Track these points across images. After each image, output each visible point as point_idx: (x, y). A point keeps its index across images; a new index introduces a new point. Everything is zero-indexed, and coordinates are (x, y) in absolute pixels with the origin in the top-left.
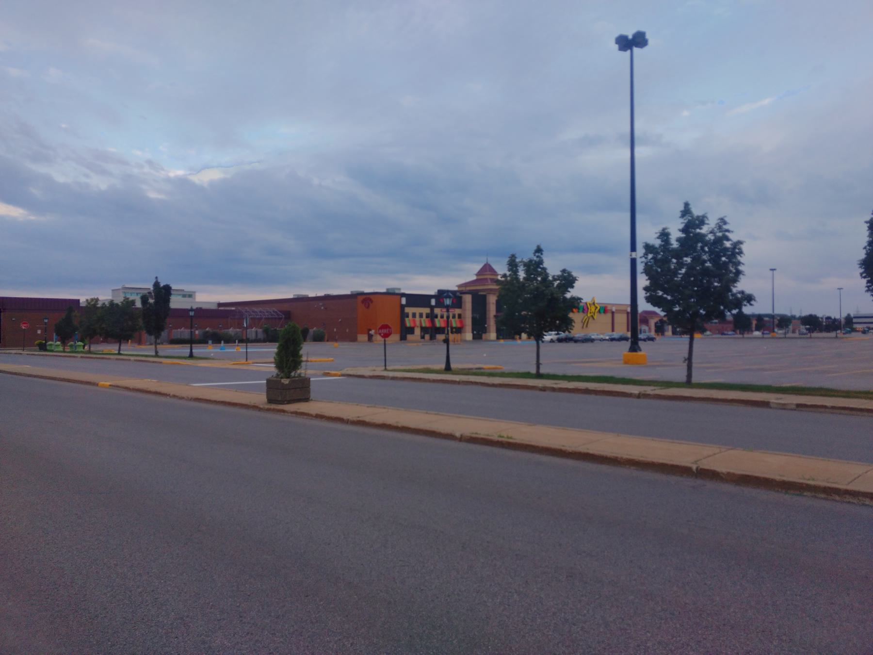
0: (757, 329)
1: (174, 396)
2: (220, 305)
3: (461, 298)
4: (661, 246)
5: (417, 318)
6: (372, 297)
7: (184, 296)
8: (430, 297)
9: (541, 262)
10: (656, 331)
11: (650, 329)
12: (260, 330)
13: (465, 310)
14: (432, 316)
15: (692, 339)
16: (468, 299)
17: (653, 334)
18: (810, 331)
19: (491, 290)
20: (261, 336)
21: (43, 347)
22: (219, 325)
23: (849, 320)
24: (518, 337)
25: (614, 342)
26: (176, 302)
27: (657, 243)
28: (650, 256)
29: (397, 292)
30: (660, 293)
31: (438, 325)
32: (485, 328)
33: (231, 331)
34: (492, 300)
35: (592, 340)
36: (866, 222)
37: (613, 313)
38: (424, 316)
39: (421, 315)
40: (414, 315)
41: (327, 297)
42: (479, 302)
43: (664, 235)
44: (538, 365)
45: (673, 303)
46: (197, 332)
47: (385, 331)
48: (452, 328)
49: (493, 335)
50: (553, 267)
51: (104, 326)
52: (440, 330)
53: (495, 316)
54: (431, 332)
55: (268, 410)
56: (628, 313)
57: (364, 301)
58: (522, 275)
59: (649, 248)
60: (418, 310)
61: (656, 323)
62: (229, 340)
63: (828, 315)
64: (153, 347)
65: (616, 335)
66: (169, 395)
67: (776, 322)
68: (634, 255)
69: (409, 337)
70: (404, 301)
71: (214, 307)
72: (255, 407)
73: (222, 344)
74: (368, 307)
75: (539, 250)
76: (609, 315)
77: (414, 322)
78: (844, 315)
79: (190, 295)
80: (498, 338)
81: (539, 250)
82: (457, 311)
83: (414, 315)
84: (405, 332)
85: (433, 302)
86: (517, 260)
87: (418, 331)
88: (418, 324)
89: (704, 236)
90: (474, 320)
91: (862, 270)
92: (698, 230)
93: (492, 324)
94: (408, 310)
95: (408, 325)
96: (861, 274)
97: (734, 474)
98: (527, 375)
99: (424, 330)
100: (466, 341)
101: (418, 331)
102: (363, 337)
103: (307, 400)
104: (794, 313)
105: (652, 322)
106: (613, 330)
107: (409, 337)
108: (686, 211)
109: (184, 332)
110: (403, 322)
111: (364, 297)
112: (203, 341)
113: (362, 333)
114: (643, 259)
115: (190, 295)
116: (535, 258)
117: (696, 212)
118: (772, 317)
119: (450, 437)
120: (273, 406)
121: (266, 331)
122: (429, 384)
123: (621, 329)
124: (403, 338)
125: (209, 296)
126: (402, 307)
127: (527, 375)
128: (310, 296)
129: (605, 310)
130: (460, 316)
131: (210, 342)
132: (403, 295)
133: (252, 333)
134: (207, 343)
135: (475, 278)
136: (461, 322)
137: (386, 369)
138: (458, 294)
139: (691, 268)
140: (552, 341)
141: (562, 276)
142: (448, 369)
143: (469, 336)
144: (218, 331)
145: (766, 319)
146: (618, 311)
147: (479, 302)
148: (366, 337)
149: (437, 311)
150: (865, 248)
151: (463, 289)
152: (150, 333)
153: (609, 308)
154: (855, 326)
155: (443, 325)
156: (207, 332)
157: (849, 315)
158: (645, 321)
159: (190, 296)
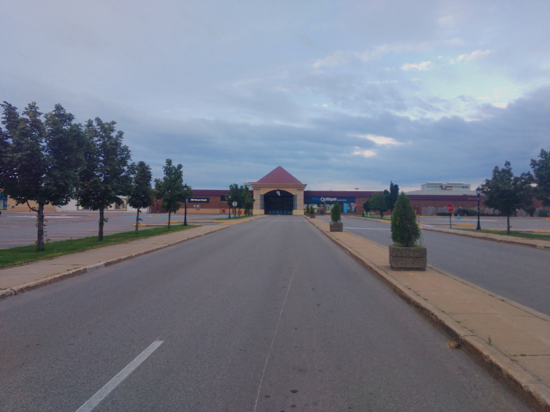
7: (463, 187)
15: (169, 223)
21: (363, 215)
22: (339, 205)
44: (509, 227)
47: (450, 208)
64: (171, 224)
73: (459, 216)
79: (467, 187)
98: (501, 233)
115: (467, 187)
116: (505, 168)
127: (501, 233)
137: (451, 228)
142: (479, 228)
144: (465, 208)
159: (467, 187)
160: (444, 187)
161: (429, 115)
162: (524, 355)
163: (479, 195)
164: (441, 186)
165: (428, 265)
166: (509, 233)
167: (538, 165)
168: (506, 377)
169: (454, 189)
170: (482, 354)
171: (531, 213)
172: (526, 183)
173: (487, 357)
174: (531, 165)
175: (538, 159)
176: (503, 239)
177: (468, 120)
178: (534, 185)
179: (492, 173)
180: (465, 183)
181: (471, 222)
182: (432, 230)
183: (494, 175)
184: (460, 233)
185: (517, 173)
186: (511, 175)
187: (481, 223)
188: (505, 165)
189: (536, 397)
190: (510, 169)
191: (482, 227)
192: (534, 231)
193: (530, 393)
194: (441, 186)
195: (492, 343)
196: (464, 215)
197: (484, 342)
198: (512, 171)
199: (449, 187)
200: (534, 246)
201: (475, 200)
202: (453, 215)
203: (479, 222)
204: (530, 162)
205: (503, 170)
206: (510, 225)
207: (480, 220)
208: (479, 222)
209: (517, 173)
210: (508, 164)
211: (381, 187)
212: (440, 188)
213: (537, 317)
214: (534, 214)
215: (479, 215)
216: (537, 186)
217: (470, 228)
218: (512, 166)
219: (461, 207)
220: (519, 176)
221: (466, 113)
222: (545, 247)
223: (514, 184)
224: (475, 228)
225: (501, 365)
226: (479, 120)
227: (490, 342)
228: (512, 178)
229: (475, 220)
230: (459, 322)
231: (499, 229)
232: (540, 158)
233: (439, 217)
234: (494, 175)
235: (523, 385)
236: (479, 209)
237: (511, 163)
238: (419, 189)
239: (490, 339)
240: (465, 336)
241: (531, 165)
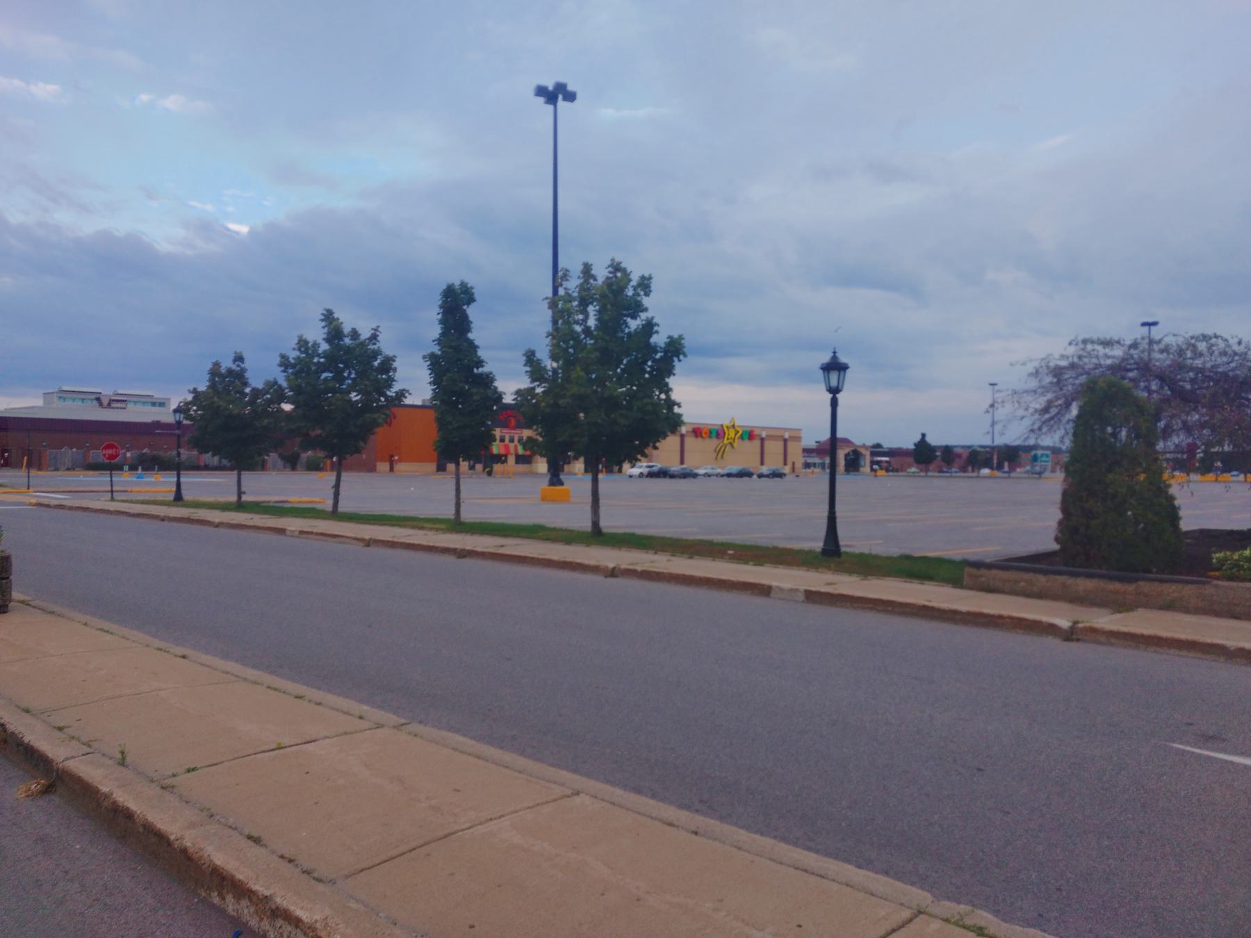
7: (154, 404)
24: (616, 468)
25: (731, 479)
35: (695, 476)
37: (762, 440)
46: (128, 455)
47: (110, 452)
61: (846, 456)
65: (765, 470)
76: (757, 443)
77: (507, 447)
88: (512, 450)
98: (225, 507)
102: (383, 466)
106: (762, 463)
107: (497, 467)
113: (382, 460)
116: (234, 367)
122: (92, 514)
127: (225, 507)
129: (751, 436)
137: (113, 499)
140: (641, 475)
142: (178, 497)
144: (161, 453)
146: (771, 437)
153: (756, 432)
160: (105, 402)
161: (63, 217)
162: (193, 770)
163: (179, 423)
164: (98, 399)
165: (16, 595)
166: (240, 506)
167: (293, 366)
168: (141, 830)
169: (130, 406)
170: (98, 791)
171: (292, 462)
172: (270, 402)
173: (107, 796)
174: (280, 365)
175: (293, 355)
176: (225, 521)
177: (164, 247)
178: (287, 407)
179: (207, 377)
180: (158, 395)
181: (162, 483)
182: (61, 507)
183: (212, 380)
184: (131, 511)
185: (256, 381)
186: (246, 384)
187: (183, 486)
188: (235, 361)
189: (195, 856)
190: (243, 370)
191: (187, 496)
192: (290, 499)
193: (184, 851)
194: (98, 399)
195: (128, 760)
196: (153, 469)
197: (110, 762)
198: (247, 375)
199: (119, 401)
200: (281, 531)
201: (172, 434)
202: (126, 468)
203: (178, 484)
204: (278, 360)
205: (230, 371)
206: (243, 489)
207: (182, 479)
208: (178, 484)
209: (256, 381)
210: (239, 358)
212: (95, 403)
213: (245, 680)
214: (298, 466)
215: (177, 467)
216: (294, 410)
217: (160, 498)
218: (246, 365)
220: (260, 386)
221: (162, 232)
222: (301, 532)
223: (252, 403)
224: (171, 497)
225: (133, 805)
226: (189, 252)
227: (124, 759)
228: (248, 390)
229: (169, 479)
230: (60, 729)
231: (222, 499)
232: (297, 353)
233: (91, 473)
234: (210, 380)
235: (172, 838)
236: (179, 454)
237: (245, 356)
238: (39, 402)
239: (123, 753)
240: (67, 759)
241: (280, 365)
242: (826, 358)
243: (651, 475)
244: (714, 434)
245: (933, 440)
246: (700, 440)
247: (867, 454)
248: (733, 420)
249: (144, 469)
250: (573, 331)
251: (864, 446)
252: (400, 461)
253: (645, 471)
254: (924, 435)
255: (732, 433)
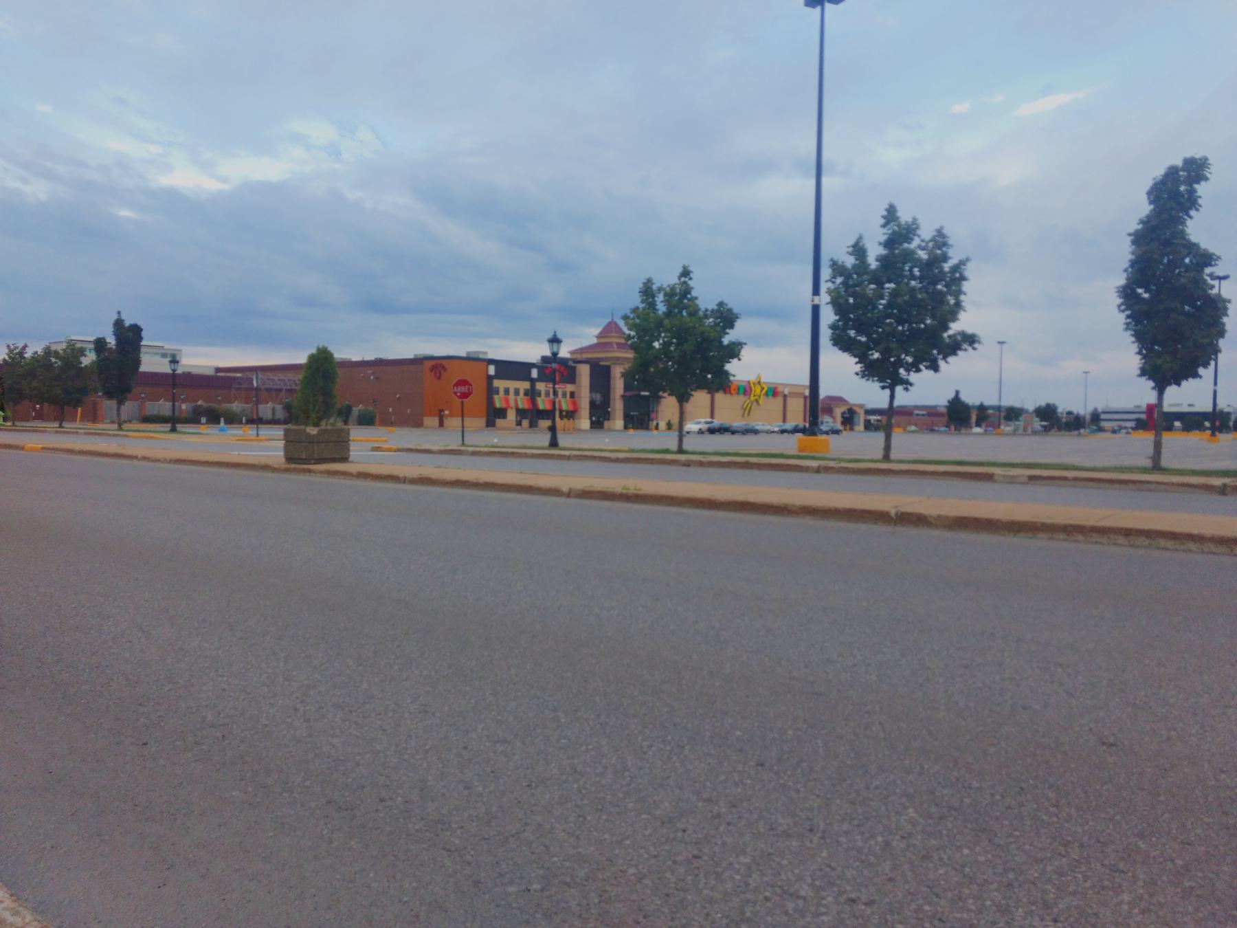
0: (978, 424)
1: (144, 458)
2: (218, 370)
3: (574, 369)
4: (854, 266)
5: (512, 397)
6: (445, 363)
8: (532, 365)
9: (687, 291)
10: (843, 423)
11: (834, 418)
12: (279, 407)
13: (580, 386)
14: (532, 394)
16: (584, 371)
17: (839, 426)
18: (1046, 429)
19: (618, 359)
20: (280, 414)
23: (1096, 417)
26: (151, 363)
27: (850, 261)
28: (839, 280)
29: (481, 356)
30: (852, 333)
31: (541, 406)
32: (609, 413)
33: (236, 406)
34: (617, 372)
36: (1130, 235)
37: (785, 397)
38: (522, 393)
39: (517, 392)
40: (507, 391)
41: (379, 362)
42: (601, 376)
43: (859, 250)
45: (867, 348)
46: (184, 407)
48: (561, 411)
49: (619, 423)
50: (706, 297)
51: (35, 384)
52: (548, 414)
53: (623, 396)
54: (532, 415)
55: (287, 470)
56: (805, 397)
57: (433, 369)
58: (661, 308)
59: (838, 269)
60: (513, 385)
61: (843, 414)
62: (232, 420)
63: (1069, 409)
65: (789, 425)
66: (136, 457)
67: (1003, 414)
68: (817, 300)
69: (499, 422)
70: (492, 370)
71: (211, 372)
72: (266, 468)
74: (439, 378)
75: (686, 273)
76: (780, 400)
77: (507, 401)
78: (1090, 409)
80: (626, 428)
81: (686, 273)
82: (569, 388)
83: (507, 391)
84: (494, 415)
85: (534, 373)
86: (655, 287)
87: (511, 415)
88: (512, 404)
89: (913, 252)
90: (593, 404)
91: (1120, 301)
92: (906, 245)
93: (618, 407)
94: (499, 384)
95: (498, 405)
96: (1119, 306)
97: (947, 517)
98: (1145, 470)
99: (521, 413)
100: (580, 430)
101: (511, 415)
102: (432, 421)
103: (345, 459)
104: (1026, 406)
105: (838, 412)
107: (499, 422)
108: (891, 215)
109: (163, 407)
110: (490, 401)
111: (434, 362)
112: (194, 419)
113: (431, 415)
114: (830, 285)
117: (904, 216)
118: (998, 408)
119: (556, 492)
120: (293, 466)
121: (288, 408)
123: (797, 417)
124: (490, 424)
125: (201, 358)
126: (490, 379)
127: (1145, 470)
128: (354, 359)
129: (774, 392)
130: (572, 395)
131: (203, 420)
132: (491, 361)
133: (266, 410)
134: (199, 422)
135: (595, 341)
136: (574, 404)
138: (571, 363)
139: (894, 294)
140: (701, 432)
141: (718, 311)
143: (585, 423)
144: (214, 405)
145: (990, 411)
147: (601, 376)
148: (436, 421)
149: (541, 386)
150: (1126, 270)
151: (578, 356)
152: (109, 395)
153: (780, 390)
154: (1104, 424)
155: (549, 407)
156: (200, 406)
157: (1096, 409)
158: (829, 411)
211: (86, 327)
219: (200, 403)
242: (550, 336)
243: (712, 431)
244: (741, 390)
245: (966, 398)
246: (728, 396)
247: (862, 412)
248: (759, 376)
249: (227, 422)
250: (1178, 190)
251: (861, 406)
252: (451, 415)
253: (705, 427)
254: (957, 392)
255: (758, 390)
